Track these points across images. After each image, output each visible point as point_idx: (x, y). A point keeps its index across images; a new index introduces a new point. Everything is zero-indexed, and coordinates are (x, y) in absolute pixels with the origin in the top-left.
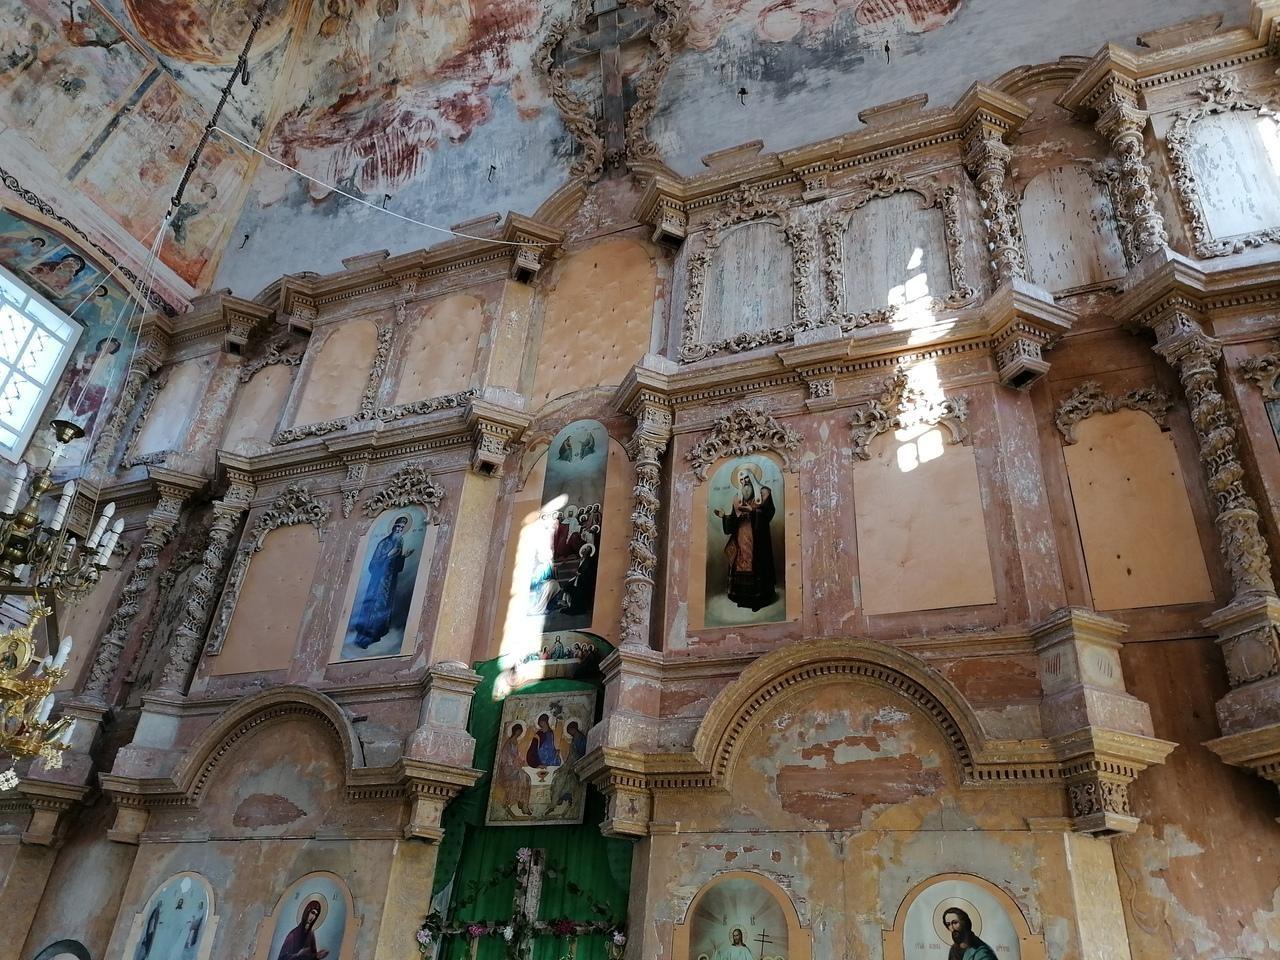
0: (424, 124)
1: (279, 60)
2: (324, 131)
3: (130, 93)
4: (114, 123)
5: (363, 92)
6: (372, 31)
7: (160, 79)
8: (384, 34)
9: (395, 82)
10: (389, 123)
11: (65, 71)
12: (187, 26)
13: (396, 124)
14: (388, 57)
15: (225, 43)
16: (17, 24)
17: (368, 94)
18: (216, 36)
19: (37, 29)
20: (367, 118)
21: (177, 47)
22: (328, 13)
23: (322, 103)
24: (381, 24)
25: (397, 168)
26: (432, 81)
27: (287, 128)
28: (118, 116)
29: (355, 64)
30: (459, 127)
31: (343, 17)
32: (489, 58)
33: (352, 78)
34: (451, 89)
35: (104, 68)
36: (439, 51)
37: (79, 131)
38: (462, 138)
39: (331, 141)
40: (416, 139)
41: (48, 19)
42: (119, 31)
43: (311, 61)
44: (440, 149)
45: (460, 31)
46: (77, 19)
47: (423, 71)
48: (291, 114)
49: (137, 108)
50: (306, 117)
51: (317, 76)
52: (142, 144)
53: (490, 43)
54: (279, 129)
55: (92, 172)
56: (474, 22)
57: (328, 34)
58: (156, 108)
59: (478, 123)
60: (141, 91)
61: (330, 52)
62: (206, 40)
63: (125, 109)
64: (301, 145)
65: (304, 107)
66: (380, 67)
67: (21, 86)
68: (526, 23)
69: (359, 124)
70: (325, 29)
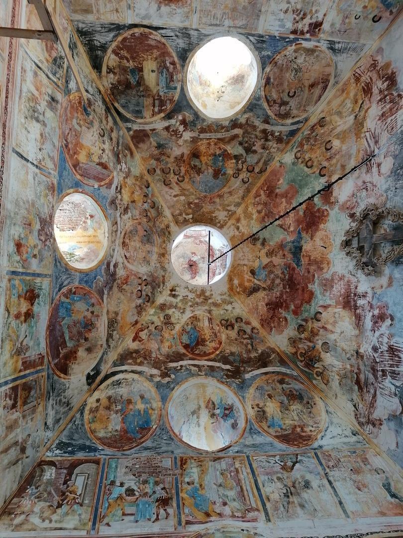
0: (380, 340)
1: (331, 409)
2: (368, 398)
3: (320, 468)
4: (330, 482)
5: (357, 371)
6: (333, 358)
7: (319, 454)
8: (336, 352)
9: (357, 352)
10: (374, 359)
11: (300, 483)
12: (303, 431)
13: (376, 355)
14: (346, 353)
15: (316, 423)
16: (274, 483)
17: (359, 369)
18: (312, 424)
19: (279, 479)
20: (369, 371)
21: (309, 440)
22: (320, 378)
23: (356, 396)
24: (332, 353)
25: (397, 359)
26: (362, 332)
27: (362, 420)
28: (328, 479)
29: (344, 371)
30: (386, 320)
31: (324, 371)
32: (361, 302)
33: (350, 375)
34: (368, 323)
35: (305, 469)
36: (351, 327)
37: (326, 496)
38: (392, 319)
39: (375, 396)
40: (386, 345)
41: (277, 473)
42: (294, 454)
43: (336, 395)
44: (393, 332)
45: (345, 315)
46: (282, 464)
47: (357, 336)
48: (356, 415)
49: (328, 470)
50: (360, 406)
51: (344, 394)
52: (345, 479)
53: (354, 301)
54: (361, 424)
55: (350, 507)
56: (344, 308)
57: (328, 381)
58: (331, 464)
59: (387, 310)
60: (321, 464)
61: (335, 383)
62: (311, 428)
63: (326, 474)
64: (372, 414)
65: (355, 406)
66: (349, 359)
67: (298, 501)
68: (352, 283)
69: (371, 376)
70: (325, 382)
